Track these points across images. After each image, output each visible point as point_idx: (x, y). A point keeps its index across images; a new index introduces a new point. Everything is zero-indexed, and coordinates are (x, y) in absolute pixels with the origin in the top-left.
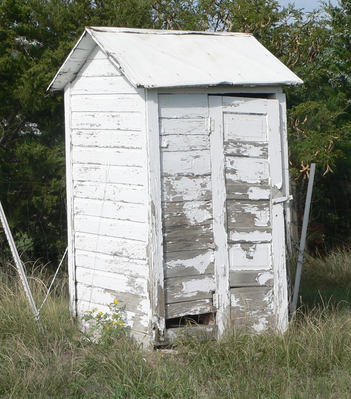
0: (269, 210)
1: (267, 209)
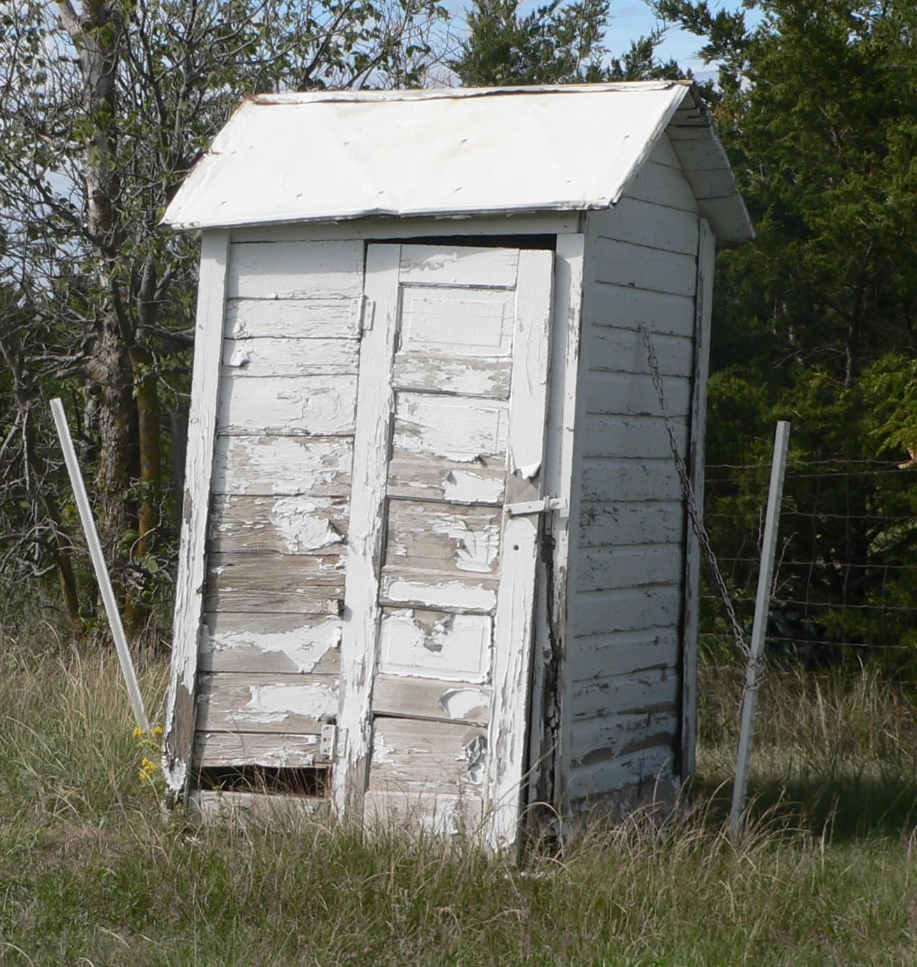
0: (499, 533)
1: (495, 529)
